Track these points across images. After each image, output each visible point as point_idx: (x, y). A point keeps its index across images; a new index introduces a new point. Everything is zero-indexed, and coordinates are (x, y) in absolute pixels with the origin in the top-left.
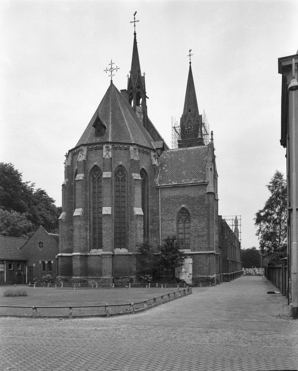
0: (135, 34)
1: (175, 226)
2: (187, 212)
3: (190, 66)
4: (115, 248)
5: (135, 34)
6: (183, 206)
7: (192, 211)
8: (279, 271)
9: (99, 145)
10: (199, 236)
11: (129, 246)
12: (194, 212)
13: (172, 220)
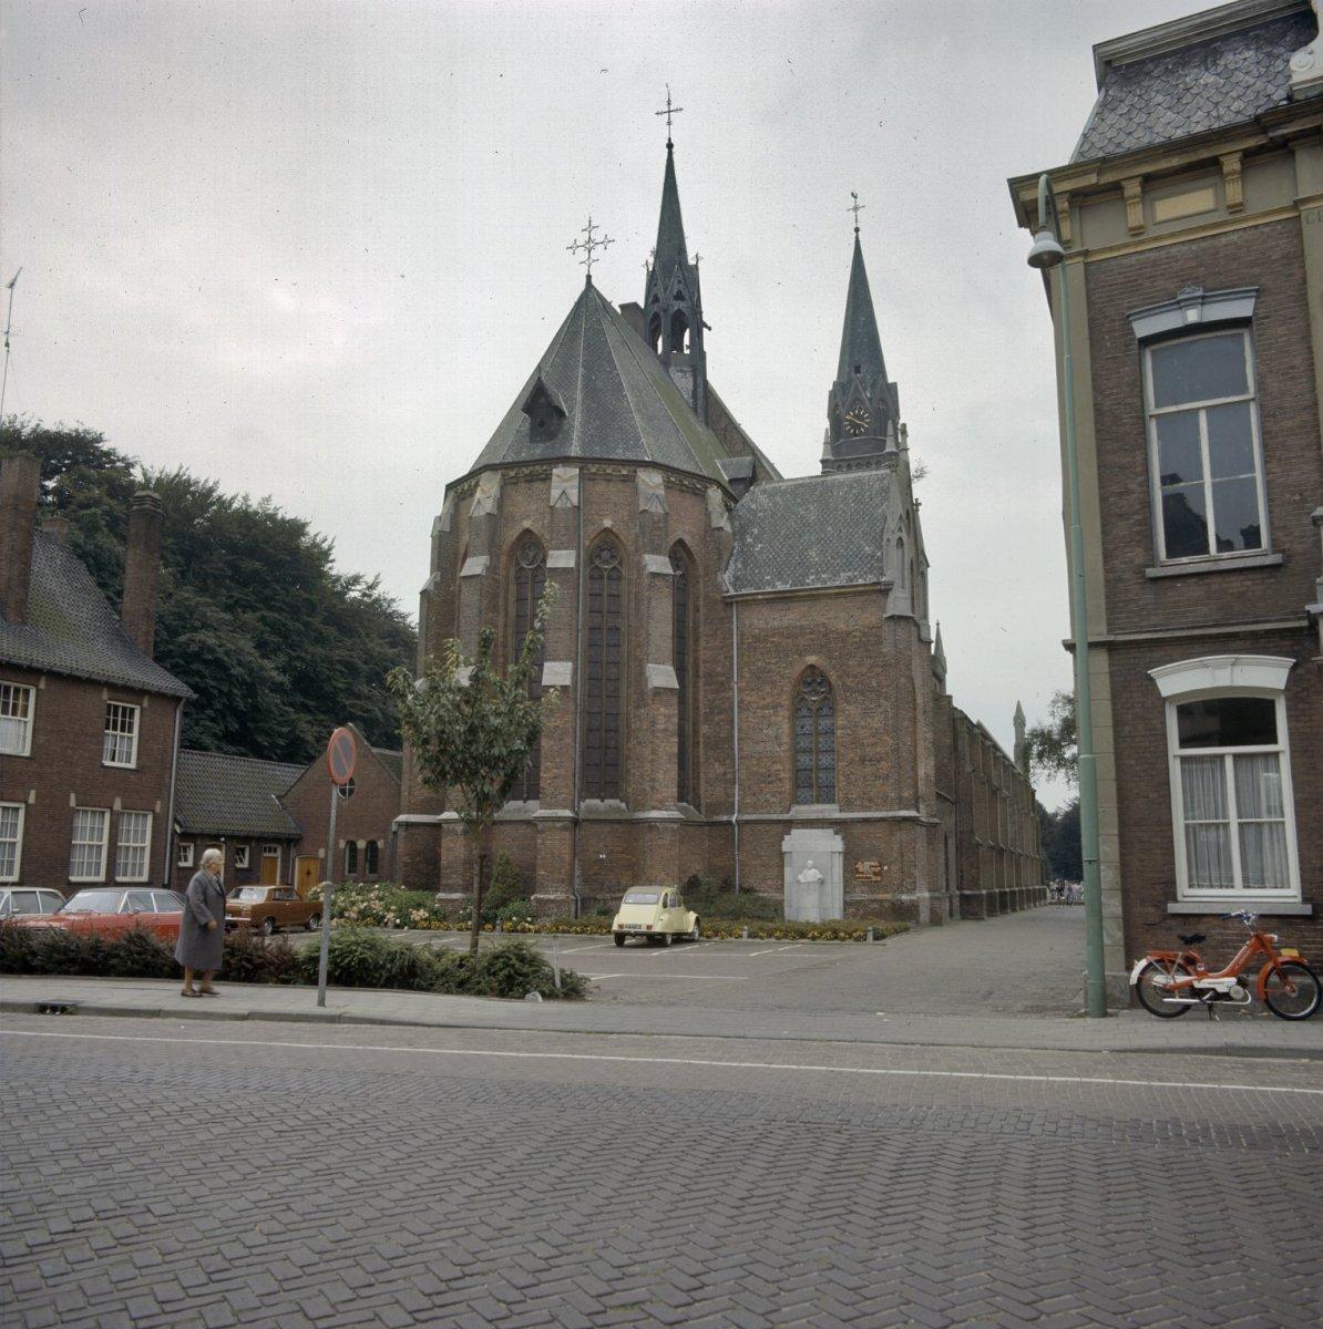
1: (786, 727)
2: (825, 681)
5: (670, 146)
6: (812, 659)
7: (839, 677)
10: (863, 760)
12: (849, 682)
13: (776, 707)
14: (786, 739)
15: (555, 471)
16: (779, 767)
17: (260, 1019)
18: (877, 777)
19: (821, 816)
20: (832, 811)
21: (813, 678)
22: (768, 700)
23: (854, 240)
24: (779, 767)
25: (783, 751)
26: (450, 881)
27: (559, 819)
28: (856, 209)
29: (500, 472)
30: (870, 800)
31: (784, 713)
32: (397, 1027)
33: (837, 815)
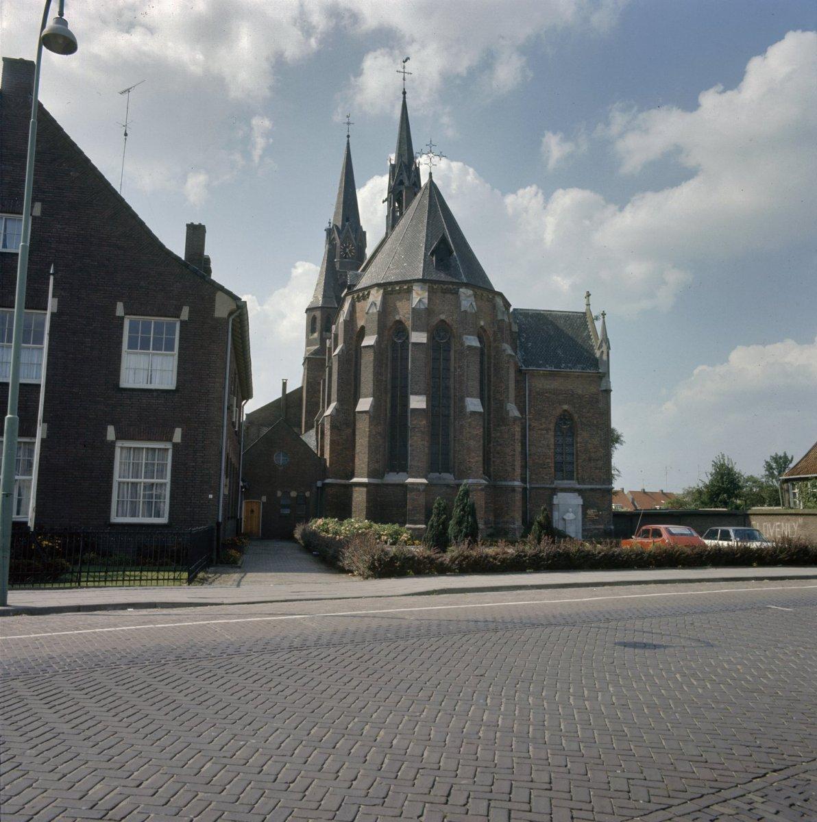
0: (404, 93)
1: (552, 440)
2: (571, 419)
3: (348, 141)
4: (429, 473)
5: (404, 93)
6: (565, 407)
7: (579, 417)
8: (744, 519)
9: (451, 286)
10: (590, 460)
11: (492, 469)
12: (583, 420)
13: (547, 430)
14: (552, 447)
15: (461, 290)
16: (549, 461)
17: (162, 608)
18: (596, 468)
19: (570, 486)
20: (573, 484)
21: (565, 418)
22: (544, 426)
23: (346, 142)
24: (549, 461)
25: (551, 453)
26: (415, 518)
27: (481, 485)
28: (349, 124)
29: (428, 284)
30: (593, 479)
31: (552, 433)
32: (165, 611)
33: (578, 486)
